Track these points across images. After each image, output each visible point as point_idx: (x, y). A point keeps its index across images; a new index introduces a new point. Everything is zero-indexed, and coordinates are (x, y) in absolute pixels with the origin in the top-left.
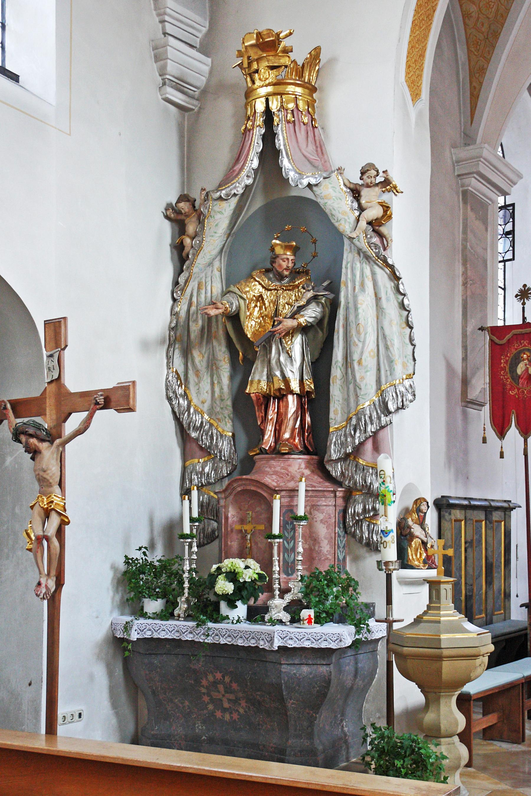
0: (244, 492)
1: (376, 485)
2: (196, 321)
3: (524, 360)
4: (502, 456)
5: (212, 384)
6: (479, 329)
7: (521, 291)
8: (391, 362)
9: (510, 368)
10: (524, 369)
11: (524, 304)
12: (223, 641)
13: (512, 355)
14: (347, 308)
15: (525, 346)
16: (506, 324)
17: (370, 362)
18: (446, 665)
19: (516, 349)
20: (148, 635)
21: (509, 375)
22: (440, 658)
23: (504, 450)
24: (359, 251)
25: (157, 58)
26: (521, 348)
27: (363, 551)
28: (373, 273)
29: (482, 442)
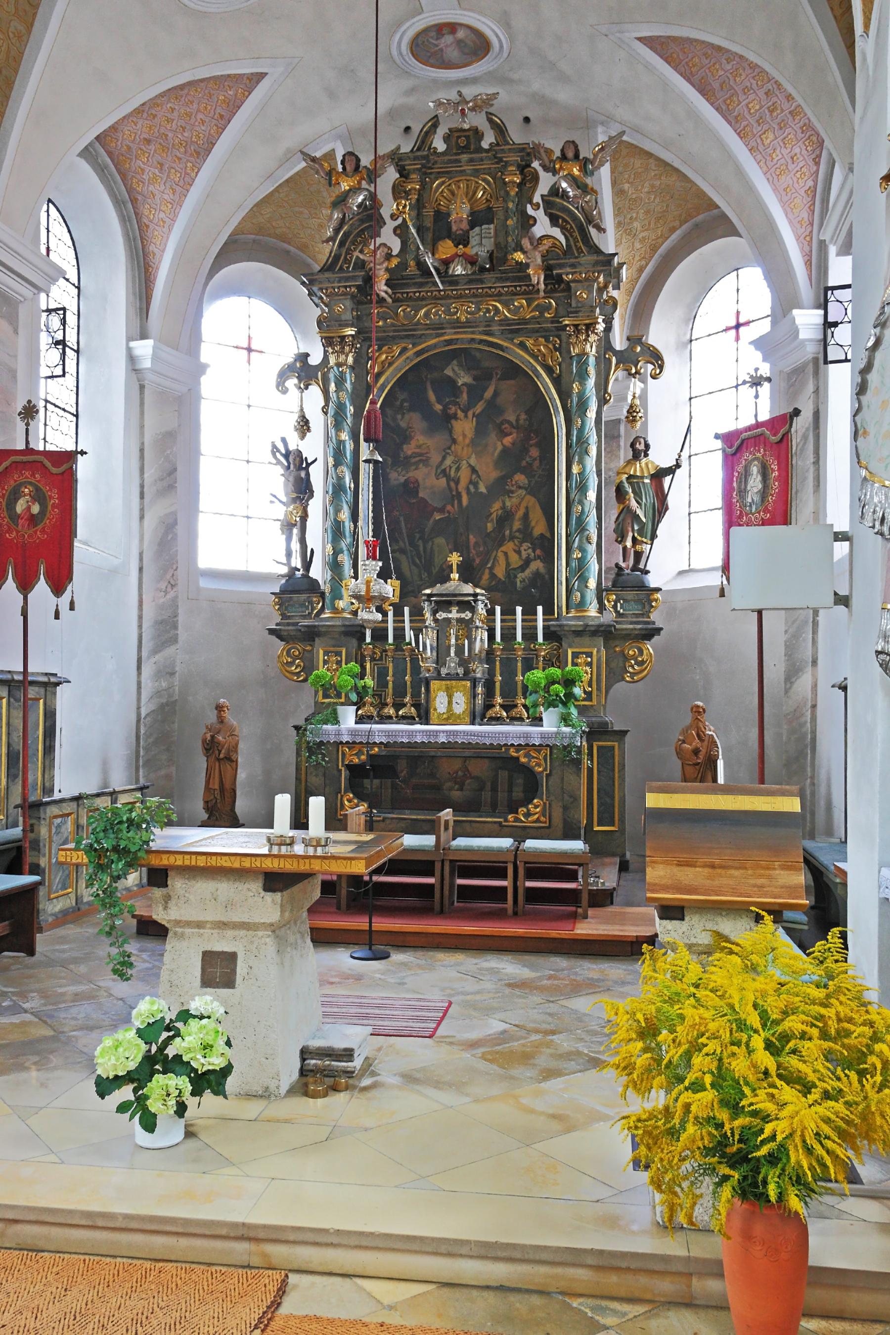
3: (25, 495)
4: (57, 617)
6: (86, 453)
7: (25, 408)
9: (7, 505)
10: (24, 507)
11: (27, 424)
13: (10, 488)
15: (27, 477)
16: (47, 449)
19: (16, 481)
21: (5, 513)
23: (59, 608)
26: (22, 480)
29: (718, 594)
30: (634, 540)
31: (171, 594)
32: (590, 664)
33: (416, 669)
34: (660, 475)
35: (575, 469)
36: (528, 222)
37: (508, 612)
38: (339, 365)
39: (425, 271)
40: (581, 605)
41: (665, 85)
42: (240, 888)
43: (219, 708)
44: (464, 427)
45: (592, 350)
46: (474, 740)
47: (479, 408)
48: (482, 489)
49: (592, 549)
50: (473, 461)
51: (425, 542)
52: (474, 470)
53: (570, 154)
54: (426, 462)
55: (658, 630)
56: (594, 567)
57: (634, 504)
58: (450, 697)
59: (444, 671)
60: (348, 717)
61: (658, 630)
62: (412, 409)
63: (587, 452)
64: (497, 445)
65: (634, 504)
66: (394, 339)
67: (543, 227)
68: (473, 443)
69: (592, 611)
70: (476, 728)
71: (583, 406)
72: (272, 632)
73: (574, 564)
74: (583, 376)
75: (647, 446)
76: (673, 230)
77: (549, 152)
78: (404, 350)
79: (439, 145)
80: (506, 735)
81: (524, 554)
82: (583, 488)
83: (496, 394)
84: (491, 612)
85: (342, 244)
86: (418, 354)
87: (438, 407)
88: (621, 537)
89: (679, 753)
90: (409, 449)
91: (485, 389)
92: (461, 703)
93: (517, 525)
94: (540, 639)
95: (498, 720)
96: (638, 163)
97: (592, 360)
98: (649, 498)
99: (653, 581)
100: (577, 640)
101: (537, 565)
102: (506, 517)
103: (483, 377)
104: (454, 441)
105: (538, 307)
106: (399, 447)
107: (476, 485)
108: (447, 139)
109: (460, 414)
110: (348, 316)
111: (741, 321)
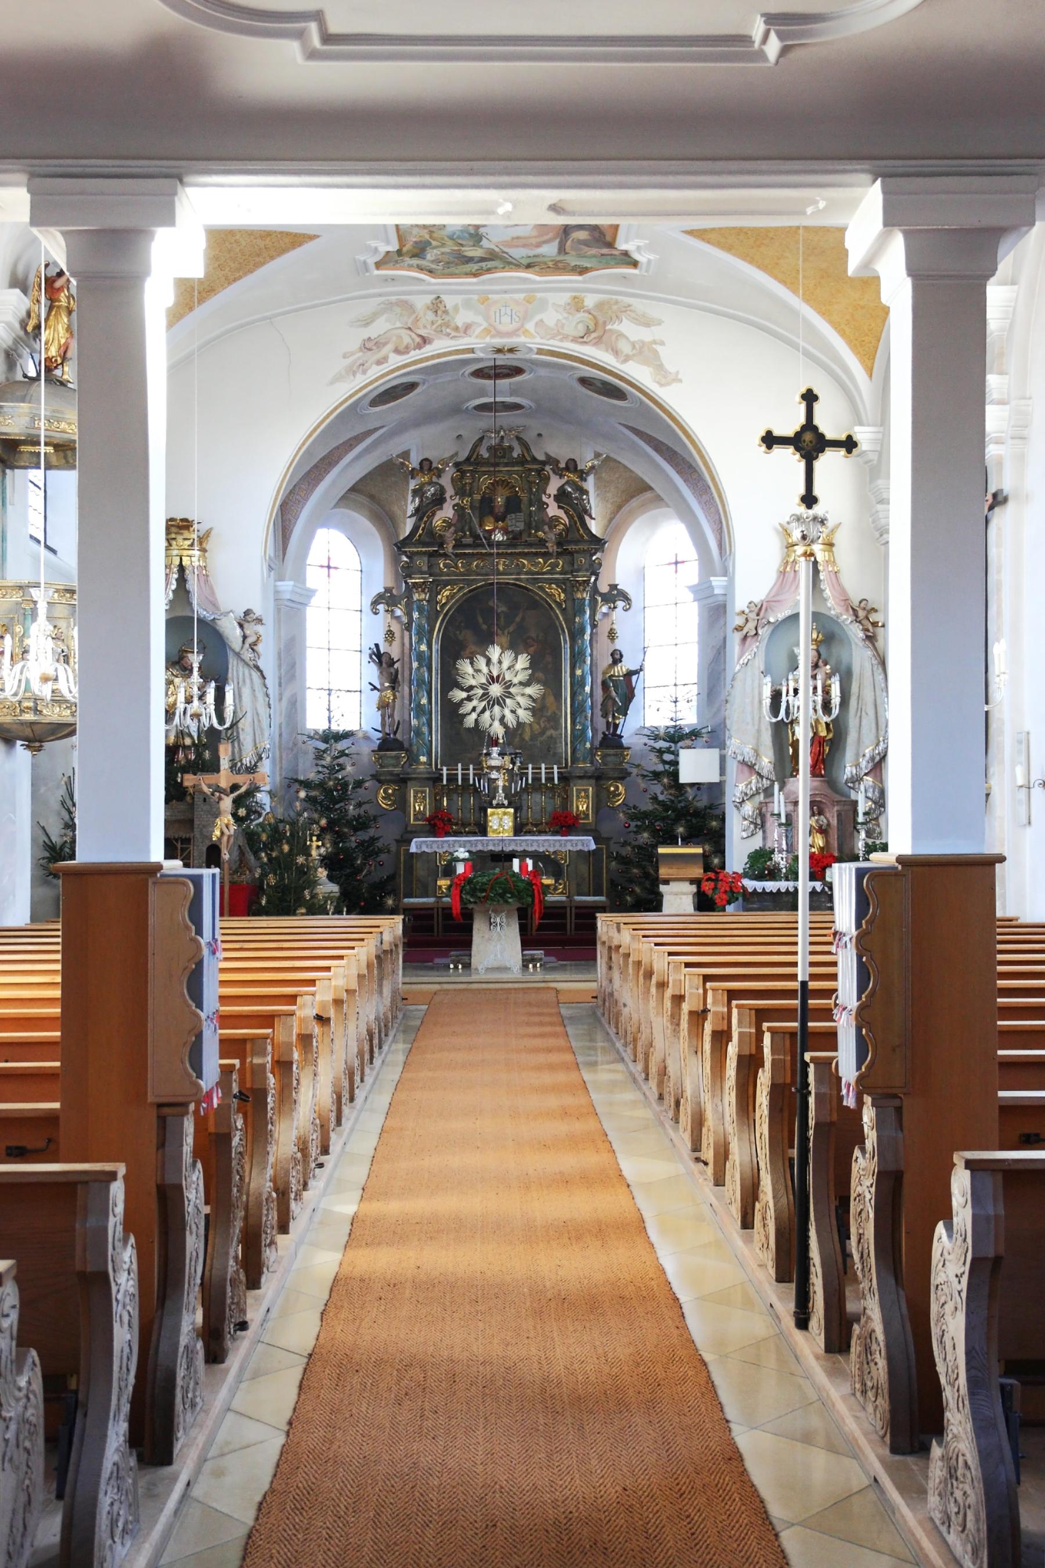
8: (262, 730)
28: (250, 675)
31: (295, 751)
34: (630, 674)
36: (542, 506)
42: (487, 936)
45: (587, 596)
47: (511, 629)
49: (588, 723)
53: (571, 466)
57: (614, 694)
63: (585, 662)
65: (614, 694)
67: (553, 510)
71: (582, 631)
75: (621, 656)
77: (558, 462)
81: (543, 725)
83: (523, 619)
86: (470, 591)
87: (484, 627)
99: (625, 741)
100: (580, 781)
111: (679, 560)
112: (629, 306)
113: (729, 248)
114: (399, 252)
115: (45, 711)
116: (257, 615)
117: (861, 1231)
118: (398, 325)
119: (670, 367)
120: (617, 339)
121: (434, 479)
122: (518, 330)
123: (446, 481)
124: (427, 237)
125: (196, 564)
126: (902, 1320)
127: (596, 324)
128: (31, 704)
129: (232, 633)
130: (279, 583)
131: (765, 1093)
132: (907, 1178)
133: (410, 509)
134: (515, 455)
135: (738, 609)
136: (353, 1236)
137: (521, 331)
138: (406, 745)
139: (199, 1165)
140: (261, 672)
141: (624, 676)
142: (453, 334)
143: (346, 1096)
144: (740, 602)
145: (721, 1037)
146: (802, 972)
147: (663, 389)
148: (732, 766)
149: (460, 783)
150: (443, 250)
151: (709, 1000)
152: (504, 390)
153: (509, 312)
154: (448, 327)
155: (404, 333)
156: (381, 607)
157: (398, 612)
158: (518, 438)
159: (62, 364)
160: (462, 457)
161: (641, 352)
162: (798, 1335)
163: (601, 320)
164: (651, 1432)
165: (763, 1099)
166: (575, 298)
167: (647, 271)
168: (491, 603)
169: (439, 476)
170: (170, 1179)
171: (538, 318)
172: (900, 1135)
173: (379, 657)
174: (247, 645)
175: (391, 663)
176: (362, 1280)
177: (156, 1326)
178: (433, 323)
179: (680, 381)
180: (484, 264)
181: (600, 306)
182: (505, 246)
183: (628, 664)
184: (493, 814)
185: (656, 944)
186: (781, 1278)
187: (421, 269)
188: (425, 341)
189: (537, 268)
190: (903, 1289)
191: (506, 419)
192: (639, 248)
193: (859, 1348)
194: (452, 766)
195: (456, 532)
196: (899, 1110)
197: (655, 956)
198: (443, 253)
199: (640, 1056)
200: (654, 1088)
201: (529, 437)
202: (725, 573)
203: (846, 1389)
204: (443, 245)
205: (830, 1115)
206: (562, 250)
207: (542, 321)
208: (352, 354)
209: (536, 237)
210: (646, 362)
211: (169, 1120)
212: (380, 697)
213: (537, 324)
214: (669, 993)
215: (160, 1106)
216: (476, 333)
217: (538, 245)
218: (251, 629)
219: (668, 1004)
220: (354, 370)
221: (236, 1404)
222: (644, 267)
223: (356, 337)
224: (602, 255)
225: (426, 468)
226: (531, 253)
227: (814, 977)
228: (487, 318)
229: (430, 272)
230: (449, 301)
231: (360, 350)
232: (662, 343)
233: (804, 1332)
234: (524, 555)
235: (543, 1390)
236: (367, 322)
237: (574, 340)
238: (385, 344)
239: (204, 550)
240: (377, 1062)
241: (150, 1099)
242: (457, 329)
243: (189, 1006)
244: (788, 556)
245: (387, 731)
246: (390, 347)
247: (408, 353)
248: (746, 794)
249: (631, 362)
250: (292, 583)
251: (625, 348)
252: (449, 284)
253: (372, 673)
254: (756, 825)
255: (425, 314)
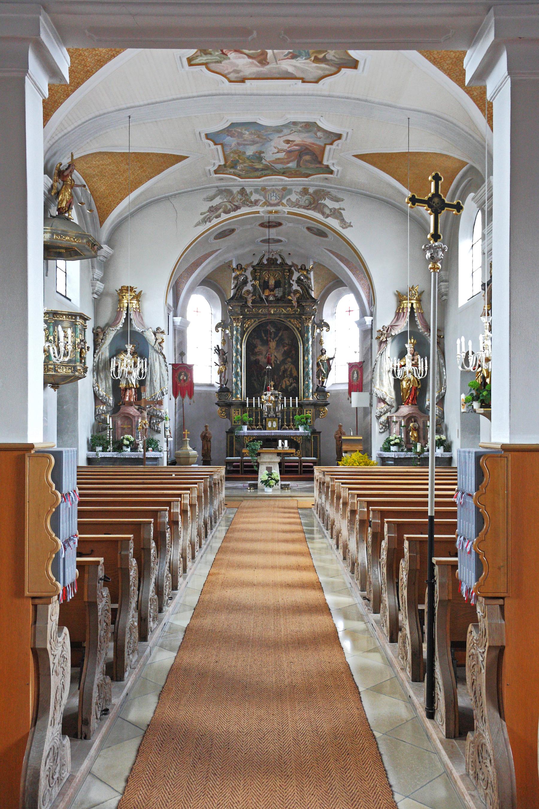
0: (124, 416)
1: (160, 414)
2: (101, 364)
5: (106, 383)
8: (164, 381)
12: (127, 457)
14: (151, 365)
17: (158, 381)
18: (190, 459)
20: (103, 456)
22: (189, 457)
24: (155, 350)
25: (92, 286)
27: (155, 433)
28: (159, 357)
30: (322, 378)
32: (310, 413)
33: (262, 415)
34: (329, 359)
35: (306, 358)
36: (291, 285)
37: (288, 398)
38: (237, 326)
39: (262, 299)
40: (308, 397)
41: (330, 256)
43: (206, 427)
44: (273, 344)
46: (282, 434)
47: (277, 339)
48: (278, 362)
49: (311, 381)
50: (275, 354)
51: (262, 378)
52: (276, 357)
53: (303, 268)
54: (262, 354)
55: (329, 404)
56: (311, 385)
57: (322, 368)
58: (272, 423)
59: (269, 415)
60: (245, 428)
61: (329, 404)
62: (257, 338)
64: (282, 350)
65: (322, 368)
66: (252, 318)
67: (295, 287)
68: (275, 349)
69: (311, 399)
70: (279, 431)
71: (308, 340)
72: (216, 404)
73: (305, 385)
74: (308, 332)
75: (325, 351)
76: (330, 282)
77: (297, 266)
78: (255, 321)
79: (266, 262)
80: (290, 433)
82: (308, 364)
83: (282, 335)
84: (283, 398)
85: (237, 290)
87: (265, 338)
88: (318, 377)
89: (335, 437)
90: (257, 350)
91: (279, 333)
92: (275, 425)
93: (289, 373)
94: (297, 406)
95: (285, 429)
96: (321, 267)
97: (310, 328)
98: (326, 366)
99: (326, 389)
101: (294, 385)
102: (285, 371)
103: (278, 330)
104: (270, 348)
105: (294, 311)
106: (253, 349)
107: (276, 361)
108: (267, 260)
109: (272, 340)
110: (239, 312)
112: (329, 192)
113: (374, 164)
114: (225, 165)
115: (59, 370)
116: (162, 330)
117: (474, 677)
118: (225, 200)
119: (347, 220)
120: (323, 207)
121: (243, 273)
122: (279, 203)
123: (248, 273)
124: (237, 158)
125: (135, 307)
126: (506, 743)
127: (314, 201)
128: (52, 367)
129: (151, 338)
130: (175, 318)
131: (405, 573)
132: (507, 651)
133: (233, 286)
134: (278, 262)
135: (378, 329)
136: (185, 640)
137: (280, 204)
138: (231, 390)
139: (66, 630)
140: (164, 356)
141: (327, 360)
142: (250, 204)
143: (189, 556)
144: (379, 326)
145: (377, 537)
146: (430, 510)
147: (345, 230)
148: (375, 400)
149: (254, 406)
150: (245, 165)
151: (371, 516)
152: (273, 233)
153: (275, 195)
154: (247, 201)
155: (227, 204)
156: (220, 329)
157: (228, 332)
158: (280, 255)
159: (68, 211)
160: (255, 263)
161: (334, 213)
162: (428, 723)
163: (316, 198)
164: (344, 794)
165: (404, 576)
166: (304, 188)
167: (337, 175)
168: (268, 328)
169: (245, 272)
170: (39, 645)
171: (288, 198)
172: (503, 622)
173: (218, 350)
174: (157, 343)
175: (224, 354)
176: (185, 670)
177: (29, 738)
178: (241, 199)
179: (352, 226)
180: (263, 172)
181: (316, 192)
182: (273, 163)
183: (328, 355)
184: (269, 421)
185: (343, 483)
186: (416, 678)
187: (235, 174)
188: (237, 208)
189: (287, 175)
190: (505, 721)
191: (274, 247)
192: (333, 164)
193: (472, 750)
194: (251, 398)
195: (252, 296)
196: (502, 607)
197: (342, 490)
198: (245, 166)
199: (335, 537)
200: (342, 554)
201: (285, 255)
202: (371, 315)
203: (463, 769)
204: (244, 162)
205: (448, 596)
206: (298, 165)
207: (290, 199)
208: (205, 213)
209: (286, 159)
210: (336, 218)
211: (39, 607)
212: (219, 368)
213: (287, 200)
214: (349, 508)
215: (33, 598)
216: (261, 204)
217: (288, 163)
218: (159, 336)
219: (348, 514)
220: (205, 220)
221: (95, 769)
222: (336, 173)
223: (205, 207)
224: (317, 168)
225: (239, 268)
226: (285, 167)
227: (439, 514)
228: (265, 198)
229: (239, 176)
230: (248, 190)
231: (208, 211)
232: (344, 209)
233: (432, 721)
234: (283, 307)
235: (280, 757)
236: (211, 199)
237: (305, 208)
238: (220, 209)
239: (138, 301)
240: (209, 537)
241: (27, 593)
242: (251, 202)
243: (51, 535)
244: (401, 305)
245: (222, 383)
246: (221, 210)
247: (230, 213)
248: (381, 412)
249: (329, 218)
250: (180, 318)
251: (328, 212)
252: (248, 181)
253: (216, 358)
254: (386, 426)
255: (237, 196)
